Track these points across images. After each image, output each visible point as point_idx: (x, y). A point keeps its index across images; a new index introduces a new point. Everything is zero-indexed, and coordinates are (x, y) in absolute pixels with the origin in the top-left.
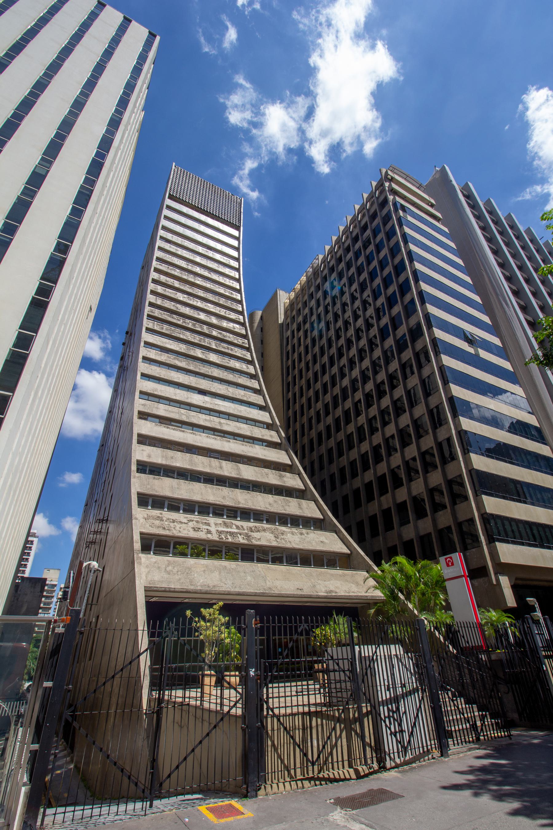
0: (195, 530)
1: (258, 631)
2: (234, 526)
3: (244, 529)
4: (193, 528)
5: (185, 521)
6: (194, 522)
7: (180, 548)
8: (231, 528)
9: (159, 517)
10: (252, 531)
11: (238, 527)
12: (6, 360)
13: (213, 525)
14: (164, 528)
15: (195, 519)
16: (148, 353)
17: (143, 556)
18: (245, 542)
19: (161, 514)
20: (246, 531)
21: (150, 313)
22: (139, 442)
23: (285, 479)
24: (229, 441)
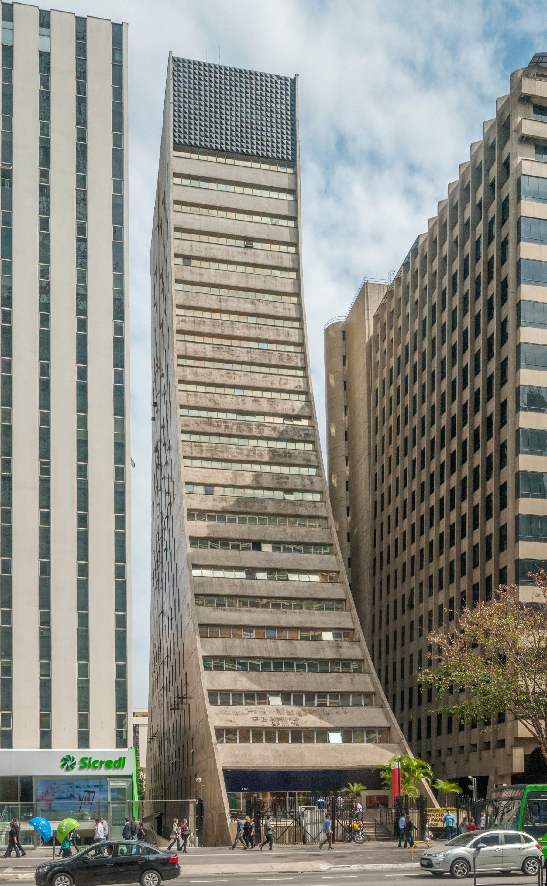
0: (254, 720)
1: (261, 701)
2: (285, 713)
3: (294, 714)
4: (252, 718)
5: (246, 712)
6: (253, 712)
7: (81, 89)
8: (283, 714)
9: (226, 711)
10: (300, 715)
11: (289, 713)
12: (506, 489)
13: (267, 713)
14: (231, 721)
15: (254, 710)
16: (192, 502)
17: (219, 746)
18: (293, 726)
19: (228, 708)
20: (295, 716)
21: (184, 428)
22: (174, 231)
23: (342, 650)
24: (286, 612)
